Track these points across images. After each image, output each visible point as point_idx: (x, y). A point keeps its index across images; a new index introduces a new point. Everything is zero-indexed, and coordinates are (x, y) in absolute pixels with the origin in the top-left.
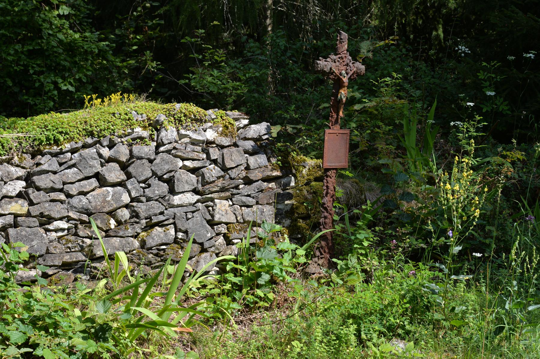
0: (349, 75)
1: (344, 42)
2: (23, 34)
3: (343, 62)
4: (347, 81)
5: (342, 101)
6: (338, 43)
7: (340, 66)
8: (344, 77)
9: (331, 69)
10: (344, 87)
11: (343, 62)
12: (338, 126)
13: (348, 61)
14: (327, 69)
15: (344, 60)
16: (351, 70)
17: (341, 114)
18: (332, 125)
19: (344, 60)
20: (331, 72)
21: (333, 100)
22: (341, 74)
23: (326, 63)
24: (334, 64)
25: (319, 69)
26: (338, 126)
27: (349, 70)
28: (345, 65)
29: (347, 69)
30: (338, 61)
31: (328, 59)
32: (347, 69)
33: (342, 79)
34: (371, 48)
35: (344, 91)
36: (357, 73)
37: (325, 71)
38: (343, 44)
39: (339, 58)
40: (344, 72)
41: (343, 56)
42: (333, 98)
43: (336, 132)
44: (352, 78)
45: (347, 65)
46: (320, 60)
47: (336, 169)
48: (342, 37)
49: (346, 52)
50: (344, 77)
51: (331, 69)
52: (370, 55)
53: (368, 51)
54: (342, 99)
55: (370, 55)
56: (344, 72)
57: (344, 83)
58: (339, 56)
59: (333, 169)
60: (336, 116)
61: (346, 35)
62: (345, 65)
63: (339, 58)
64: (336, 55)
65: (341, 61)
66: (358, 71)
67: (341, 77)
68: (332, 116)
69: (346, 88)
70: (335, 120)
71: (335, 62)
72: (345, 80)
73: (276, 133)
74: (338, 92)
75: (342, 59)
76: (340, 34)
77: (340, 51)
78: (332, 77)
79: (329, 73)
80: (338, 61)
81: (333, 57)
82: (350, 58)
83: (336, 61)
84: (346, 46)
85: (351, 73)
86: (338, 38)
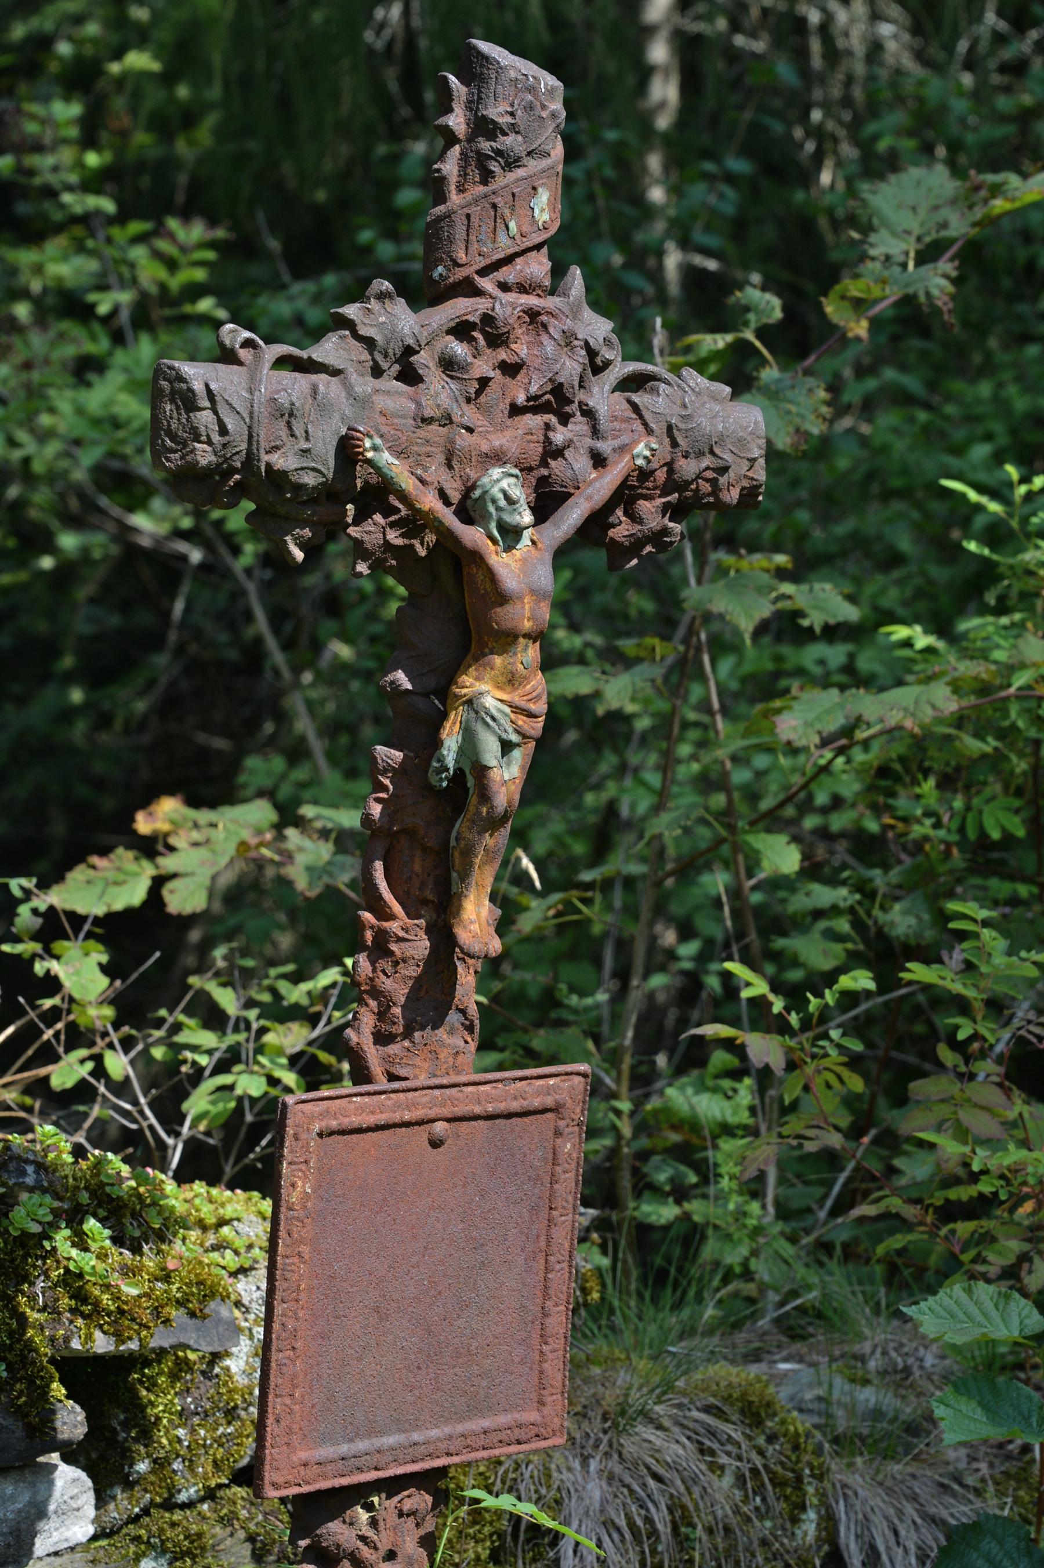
0: (572, 516)
1: (511, 163)
2: (676, 191)
3: (511, 369)
4: (544, 576)
5: (485, 796)
6: (450, 167)
7: (468, 414)
8: (511, 534)
9: (347, 451)
10: (507, 639)
11: (511, 369)
12: (453, 1042)
13: (570, 367)
14: (302, 459)
15: (521, 349)
16: (599, 461)
17: (476, 919)
18: (382, 1038)
19: (521, 349)
20: (354, 486)
21: (399, 773)
22: (470, 509)
23: (295, 386)
24: (392, 396)
25: (204, 456)
26: (453, 1042)
27: (579, 462)
28: (535, 406)
29: (553, 452)
30: (448, 365)
31: (330, 349)
32: (553, 452)
33: (477, 557)
34: (959, 226)
35: (511, 681)
36: (673, 484)
37: (277, 478)
38: (504, 179)
39: (462, 330)
40: (503, 483)
41: (508, 307)
42: (390, 755)
43: (422, 1104)
44: (622, 530)
45: (556, 402)
46: (227, 356)
47: (432, 1481)
48: (496, 112)
49: (538, 266)
50: (511, 534)
51: (347, 451)
52: (937, 282)
53: (928, 254)
54: (482, 771)
55: (937, 282)
56: (503, 483)
57: (502, 598)
58: (460, 307)
59: (392, 1486)
60: (420, 946)
61: (548, 80)
62: (535, 406)
63: (462, 330)
64: (421, 293)
65: (483, 367)
66: (688, 468)
67: (472, 535)
68: (382, 938)
69: (530, 653)
70: (418, 985)
71: (410, 376)
72: (524, 569)
73: (204, 877)
74: (440, 692)
75: (497, 340)
76: (475, 71)
77: (468, 258)
78: (373, 531)
79: (332, 494)
80: (448, 365)
81: (393, 319)
82: (598, 328)
83: (424, 360)
84: (544, 209)
85: (600, 487)
86: (457, 121)
